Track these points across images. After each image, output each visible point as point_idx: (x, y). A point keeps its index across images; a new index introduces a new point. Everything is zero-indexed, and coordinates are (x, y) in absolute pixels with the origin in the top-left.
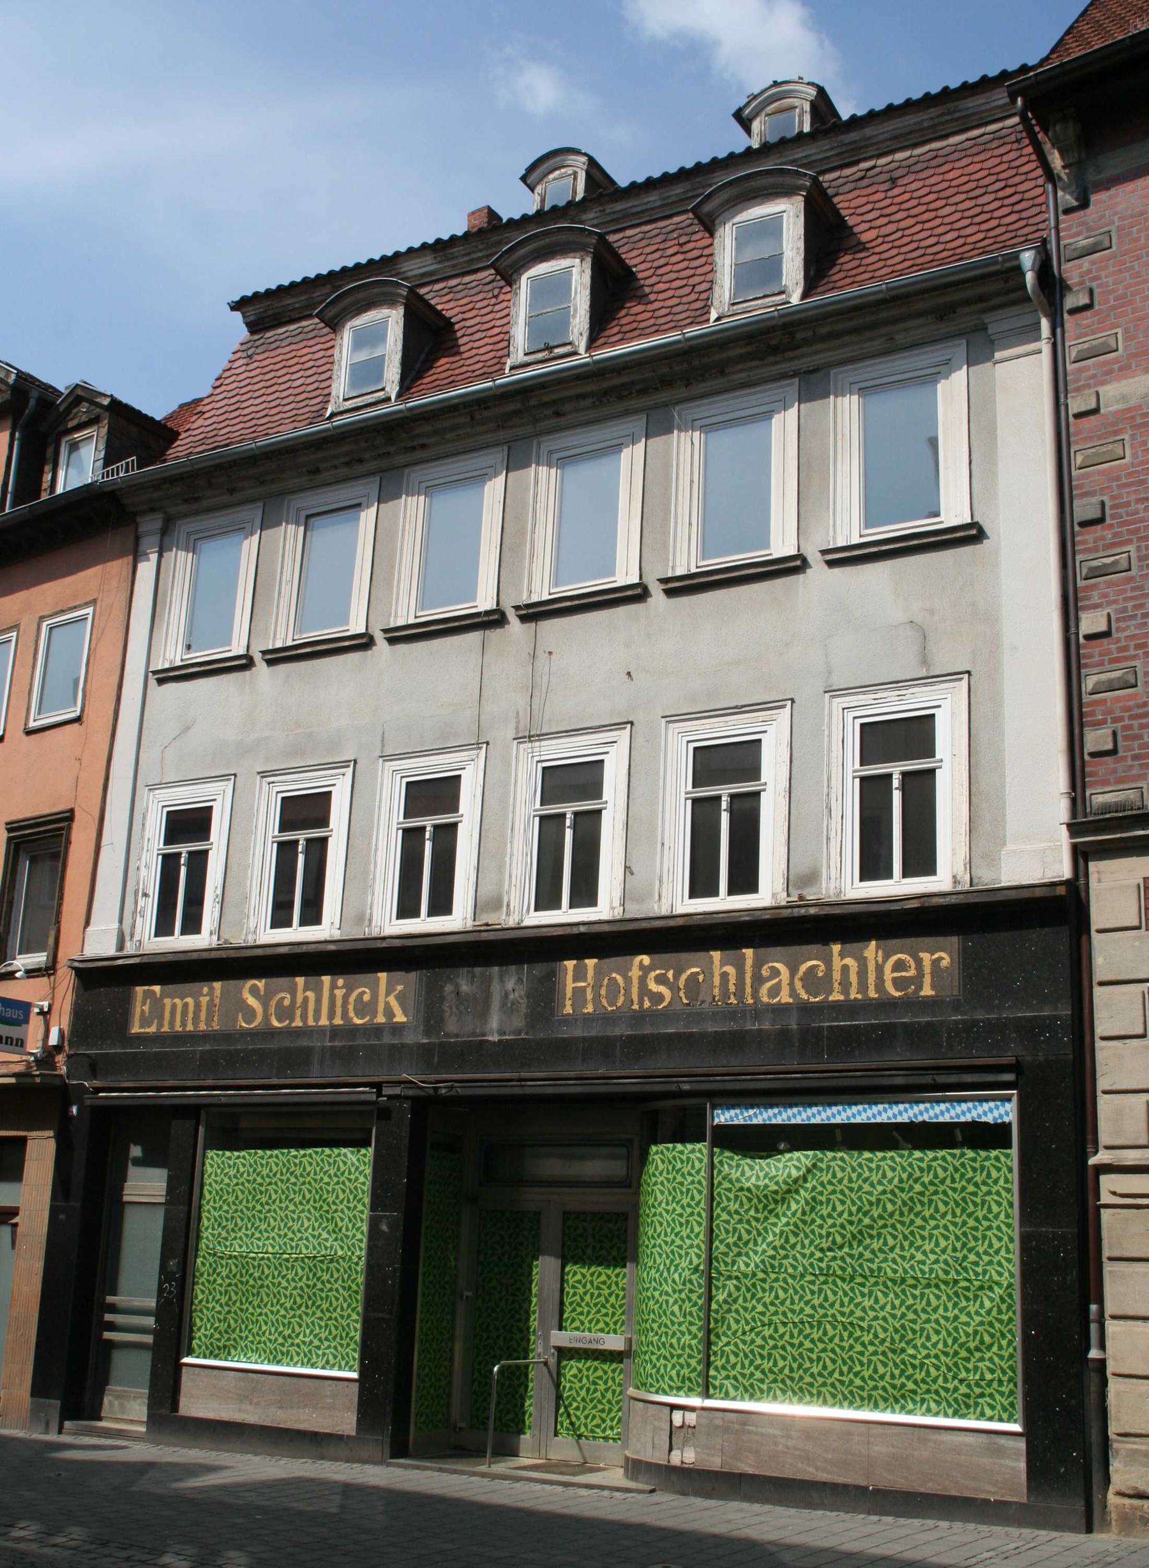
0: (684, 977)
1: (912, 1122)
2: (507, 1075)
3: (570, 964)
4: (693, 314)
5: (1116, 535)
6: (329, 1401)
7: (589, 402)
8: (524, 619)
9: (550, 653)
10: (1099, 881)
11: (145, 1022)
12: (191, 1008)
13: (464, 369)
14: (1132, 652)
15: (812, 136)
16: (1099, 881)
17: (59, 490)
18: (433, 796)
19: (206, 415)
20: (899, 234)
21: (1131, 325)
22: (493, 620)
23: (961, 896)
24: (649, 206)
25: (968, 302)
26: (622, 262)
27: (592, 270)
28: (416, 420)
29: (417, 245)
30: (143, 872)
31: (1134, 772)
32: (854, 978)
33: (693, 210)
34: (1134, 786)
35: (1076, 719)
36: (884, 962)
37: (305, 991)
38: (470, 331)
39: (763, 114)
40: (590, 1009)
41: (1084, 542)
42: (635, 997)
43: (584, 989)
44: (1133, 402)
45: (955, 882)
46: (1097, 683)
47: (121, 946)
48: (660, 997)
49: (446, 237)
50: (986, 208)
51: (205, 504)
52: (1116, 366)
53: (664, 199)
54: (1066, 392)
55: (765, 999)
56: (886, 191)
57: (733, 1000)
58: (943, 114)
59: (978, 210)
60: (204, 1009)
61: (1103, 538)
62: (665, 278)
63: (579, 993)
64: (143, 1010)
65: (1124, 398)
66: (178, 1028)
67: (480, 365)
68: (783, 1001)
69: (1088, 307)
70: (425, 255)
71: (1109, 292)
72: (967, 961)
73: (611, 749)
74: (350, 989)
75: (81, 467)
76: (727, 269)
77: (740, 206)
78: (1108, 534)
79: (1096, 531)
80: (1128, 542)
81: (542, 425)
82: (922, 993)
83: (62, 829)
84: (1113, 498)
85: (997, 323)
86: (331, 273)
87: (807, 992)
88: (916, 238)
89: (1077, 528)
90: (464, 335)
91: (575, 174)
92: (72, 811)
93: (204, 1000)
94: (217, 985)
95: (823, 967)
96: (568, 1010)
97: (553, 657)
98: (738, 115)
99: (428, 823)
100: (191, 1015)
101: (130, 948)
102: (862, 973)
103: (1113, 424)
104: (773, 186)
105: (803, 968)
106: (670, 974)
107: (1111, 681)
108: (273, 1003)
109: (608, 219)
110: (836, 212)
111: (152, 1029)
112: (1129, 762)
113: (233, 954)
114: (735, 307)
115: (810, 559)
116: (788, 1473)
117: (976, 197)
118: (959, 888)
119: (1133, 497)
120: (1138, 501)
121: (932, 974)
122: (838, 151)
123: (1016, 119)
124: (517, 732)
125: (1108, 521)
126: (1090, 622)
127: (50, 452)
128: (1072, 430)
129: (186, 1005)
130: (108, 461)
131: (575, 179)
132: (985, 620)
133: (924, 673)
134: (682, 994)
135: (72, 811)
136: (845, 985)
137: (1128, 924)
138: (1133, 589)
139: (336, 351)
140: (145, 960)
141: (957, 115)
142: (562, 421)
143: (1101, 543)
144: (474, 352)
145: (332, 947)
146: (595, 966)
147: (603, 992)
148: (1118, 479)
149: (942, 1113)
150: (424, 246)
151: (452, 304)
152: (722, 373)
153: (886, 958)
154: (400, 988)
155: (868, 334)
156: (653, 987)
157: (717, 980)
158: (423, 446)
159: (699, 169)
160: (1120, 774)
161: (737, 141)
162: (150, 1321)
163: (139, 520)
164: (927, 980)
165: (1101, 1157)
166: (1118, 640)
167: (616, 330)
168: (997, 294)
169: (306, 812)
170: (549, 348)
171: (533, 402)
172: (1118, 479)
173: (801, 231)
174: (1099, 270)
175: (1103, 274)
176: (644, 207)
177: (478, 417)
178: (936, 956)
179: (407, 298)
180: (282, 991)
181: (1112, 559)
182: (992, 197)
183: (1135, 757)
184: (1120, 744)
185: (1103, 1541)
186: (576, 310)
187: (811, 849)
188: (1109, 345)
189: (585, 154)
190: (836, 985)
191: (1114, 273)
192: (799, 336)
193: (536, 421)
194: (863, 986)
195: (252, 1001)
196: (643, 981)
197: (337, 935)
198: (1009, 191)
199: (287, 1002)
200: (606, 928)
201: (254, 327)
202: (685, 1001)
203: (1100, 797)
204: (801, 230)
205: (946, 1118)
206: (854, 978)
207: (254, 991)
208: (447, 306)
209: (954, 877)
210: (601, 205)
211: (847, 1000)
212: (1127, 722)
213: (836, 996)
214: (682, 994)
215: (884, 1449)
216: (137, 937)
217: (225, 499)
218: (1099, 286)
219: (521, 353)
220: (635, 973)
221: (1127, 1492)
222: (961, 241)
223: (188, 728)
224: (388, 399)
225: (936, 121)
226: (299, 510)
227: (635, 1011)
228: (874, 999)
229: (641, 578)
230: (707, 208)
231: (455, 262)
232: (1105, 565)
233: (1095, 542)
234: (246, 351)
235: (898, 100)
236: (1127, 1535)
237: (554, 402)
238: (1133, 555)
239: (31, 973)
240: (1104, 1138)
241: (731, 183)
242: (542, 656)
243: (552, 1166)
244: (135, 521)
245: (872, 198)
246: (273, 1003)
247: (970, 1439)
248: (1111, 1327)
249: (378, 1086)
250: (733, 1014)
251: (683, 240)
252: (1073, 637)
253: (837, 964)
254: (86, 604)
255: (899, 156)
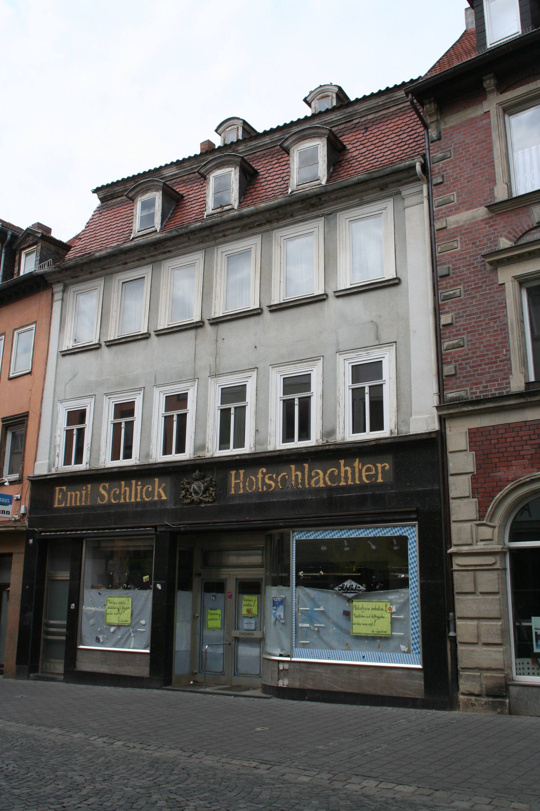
0: (280, 477)
1: (375, 537)
2: (207, 521)
3: (233, 473)
4: (282, 190)
5: (454, 281)
6: (138, 662)
7: (238, 230)
8: (211, 324)
9: (223, 339)
10: (450, 431)
11: (60, 502)
12: (79, 496)
13: (188, 217)
14: (462, 332)
15: (244, 140)
16: (450, 431)
17: (22, 274)
18: (177, 401)
19: (82, 240)
20: (368, 152)
21: (460, 191)
22: (198, 326)
23: (393, 439)
24: (265, 143)
25: (393, 182)
26: (253, 168)
27: (240, 172)
28: (166, 241)
29: (169, 163)
30: (58, 438)
31: (464, 383)
32: (349, 475)
33: (280, 145)
34: (463, 389)
35: (440, 360)
36: (362, 468)
37: (125, 487)
38: (191, 200)
39: (316, 99)
40: (242, 491)
41: (442, 285)
42: (260, 486)
43: (239, 483)
44: (461, 224)
45: (391, 433)
46: (448, 346)
47: (50, 470)
48: (270, 486)
49: (181, 159)
50: (404, 140)
51: (80, 278)
52: (454, 208)
53: (271, 139)
54: (434, 220)
55: (313, 485)
56: (363, 133)
57: (300, 486)
58: (387, 99)
59: (400, 141)
60: (84, 496)
61: (449, 283)
62: (271, 175)
63: (237, 485)
64: (59, 498)
65: (457, 222)
66: (73, 505)
67: (194, 215)
68: (321, 486)
69: (441, 183)
70: (172, 167)
71: (451, 176)
72: (396, 466)
73: (250, 380)
74: (143, 486)
75: (28, 264)
76: (295, 170)
77: (300, 143)
78: (451, 281)
79: (446, 280)
80: (460, 284)
81: (218, 241)
82: (378, 481)
83: (24, 420)
84: (453, 265)
85: (406, 191)
86: (134, 176)
87: (330, 482)
88: (374, 154)
89: (439, 279)
90: (262, 178)
91: (238, 128)
92: (28, 412)
93: (84, 492)
94: (89, 486)
95: (337, 471)
96: (233, 492)
97: (225, 340)
98: (305, 100)
99: (232, 406)
100: (78, 499)
101: (53, 471)
102: (353, 473)
103: (453, 233)
104: (314, 133)
105: (329, 472)
106: (274, 476)
107: (453, 344)
108: (112, 492)
109: (249, 148)
110: (342, 143)
111: (63, 505)
112: (462, 379)
113: (94, 472)
114: (299, 187)
115: (329, 295)
116: (326, 688)
117: (400, 135)
118: (393, 435)
119: (461, 265)
120: (464, 266)
121: (382, 472)
122: (344, 116)
123: (409, 103)
124: (210, 374)
125: (451, 275)
126: (445, 319)
127: (17, 257)
128: (436, 236)
129: (76, 495)
130: (41, 261)
131: (238, 130)
132: (403, 319)
133: (377, 343)
134: (279, 484)
135: (28, 412)
136: (346, 478)
137: (462, 449)
138: (462, 304)
139: (134, 211)
140: (59, 476)
141: (393, 99)
142: (226, 239)
143: (448, 285)
144: (192, 209)
145: (135, 468)
146: (244, 473)
147: (247, 484)
148: (455, 257)
149: (387, 532)
150: (172, 163)
151: (184, 188)
152: (292, 216)
153: (363, 467)
154: (164, 485)
155: (351, 197)
156: (267, 481)
157: (293, 478)
158: (169, 251)
159: (286, 126)
160: (458, 385)
161: (308, 112)
162: (64, 630)
163: (53, 286)
164: (380, 475)
165: (453, 549)
166: (456, 327)
167: (250, 198)
168: (405, 179)
169: (125, 410)
170: (222, 207)
171: (214, 231)
172: (455, 257)
173: (326, 153)
174: (446, 167)
175: (448, 168)
176: (263, 143)
177: (191, 238)
178: (383, 465)
179: (163, 187)
180: (116, 487)
181: (453, 292)
182: (406, 135)
183: (464, 377)
184: (458, 371)
185: (455, 714)
186: (233, 190)
187: (333, 420)
188: (450, 200)
189: (242, 120)
190: (342, 479)
191: (453, 168)
192: (323, 199)
193: (215, 239)
194: (353, 479)
195: (103, 492)
196: (263, 479)
197: (138, 463)
198: (413, 132)
199: (118, 492)
200: (247, 457)
201: (102, 200)
202: (280, 487)
203: (450, 395)
204: (325, 153)
205: (389, 534)
206: (349, 475)
207: (104, 488)
208: (181, 189)
209: (391, 431)
210: (245, 143)
211: (347, 485)
212: (460, 362)
213: (342, 483)
214: (279, 484)
215: (366, 677)
216: (56, 466)
217: (89, 276)
218: (446, 174)
219: (211, 209)
220: (260, 476)
221: (466, 693)
222: (392, 155)
223: (75, 376)
224: (156, 231)
225: (385, 102)
226: (119, 280)
227: (260, 492)
228: (358, 484)
229: (260, 306)
230: (286, 144)
231: (185, 169)
232: (450, 294)
233: (446, 284)
234: (99, 210)
235: (368, 94)
236: (466, 711)
237: (223, 231)
238: (462, 289)
239: (11, 483)
240: (454, 541)
241: (296, 133)
242: (220, 341)
243: (233, 559)
244: (52, 287)
245: (357, 137)
246: (112, 492)
247: (400, 672)
248: (459, 623)
249: (155, 527)
250: (302, 492)
251: (279, 157)
252: (438, 326)
253: (343, 469)
254: (32, 323)
255: (370, 117)
